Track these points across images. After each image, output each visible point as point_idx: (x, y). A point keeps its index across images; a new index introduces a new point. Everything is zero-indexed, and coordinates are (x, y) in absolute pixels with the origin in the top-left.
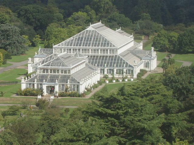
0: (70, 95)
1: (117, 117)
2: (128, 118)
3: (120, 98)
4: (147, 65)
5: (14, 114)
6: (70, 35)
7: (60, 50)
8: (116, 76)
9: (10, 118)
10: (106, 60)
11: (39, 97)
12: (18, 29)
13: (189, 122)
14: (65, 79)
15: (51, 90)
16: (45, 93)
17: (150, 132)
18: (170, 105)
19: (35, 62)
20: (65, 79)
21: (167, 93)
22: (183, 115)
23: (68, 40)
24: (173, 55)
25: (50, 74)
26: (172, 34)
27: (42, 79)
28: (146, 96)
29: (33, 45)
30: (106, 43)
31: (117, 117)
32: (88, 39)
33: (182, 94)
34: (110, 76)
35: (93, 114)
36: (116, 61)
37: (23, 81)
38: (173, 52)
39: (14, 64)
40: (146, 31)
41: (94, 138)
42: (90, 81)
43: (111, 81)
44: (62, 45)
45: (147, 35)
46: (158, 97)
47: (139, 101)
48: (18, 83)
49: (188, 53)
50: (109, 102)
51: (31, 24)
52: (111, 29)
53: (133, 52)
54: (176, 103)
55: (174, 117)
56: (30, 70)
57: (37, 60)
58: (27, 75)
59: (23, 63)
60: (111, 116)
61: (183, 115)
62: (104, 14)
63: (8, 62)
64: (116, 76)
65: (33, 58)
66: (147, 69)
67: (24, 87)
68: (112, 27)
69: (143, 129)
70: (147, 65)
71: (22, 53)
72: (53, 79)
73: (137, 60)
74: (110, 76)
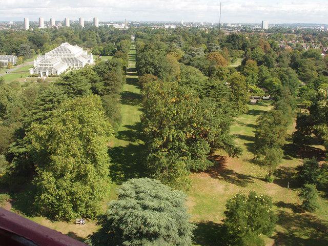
0: (53, 76)
1: (69, 85)
2: (75, 85)
3: (71, 76)
4: (89, 61)
5: (27, 86)
6: (54, 48)
7: (48, 55)
8: (75, 67)
9: (25, 88)
10: (72, 60)
11: (39, 77)
12: (29, 47)
13: (105, 86)
14: (51, 69)
15: (44, 74)
16: (42, 76)
17: (85, 91)
18: (95, 79)
19: (37, 61)
20: (51, 69)
21: (93, 74)
22: (102, 83)
23: (52, 51)
24: (101, 57)
25: (44, 66)
26: (101, 47)
27: (40, 69)
28: (85, 75)
29: (37, 54)
30: (70, 52)
31: (69, 85)
32: (61, 50)
33: (101, 74)
34: (72, 67)
35: (58, 84)
36: (75, 60)
37: (31, 70)
38: (101, 55)
39: (28, 62)
40: (89, 46)
41: (57, 95)
42: (62, 69)
43: (72, 69)
44: (49, 53)
45: (90, 48)
46: (90, 76)
47: (79, 78)
48: (29, 71)
49: (107, 55)
50: (66, 78)
51: (35, 44)
52: (236, 41)
53: (83, 56)
54: (98, 78)
55: (97, 84)
56: (35, 65)
57: (38, 61)
58: (33, 67)
59: (32, 62)
60: (67, 85)
61: (102, 83)
62: (70, 39)
63: (25, 62)
64: (75, 67)
65: (36, 59)
66: (89, 63)
67: (32, 73)
68: (74, 45)
69: (82, 90)
70: (89, 61)
71: (32, 58)
72: (45, 69)
73: (84, 59)
74: (72, 67)
